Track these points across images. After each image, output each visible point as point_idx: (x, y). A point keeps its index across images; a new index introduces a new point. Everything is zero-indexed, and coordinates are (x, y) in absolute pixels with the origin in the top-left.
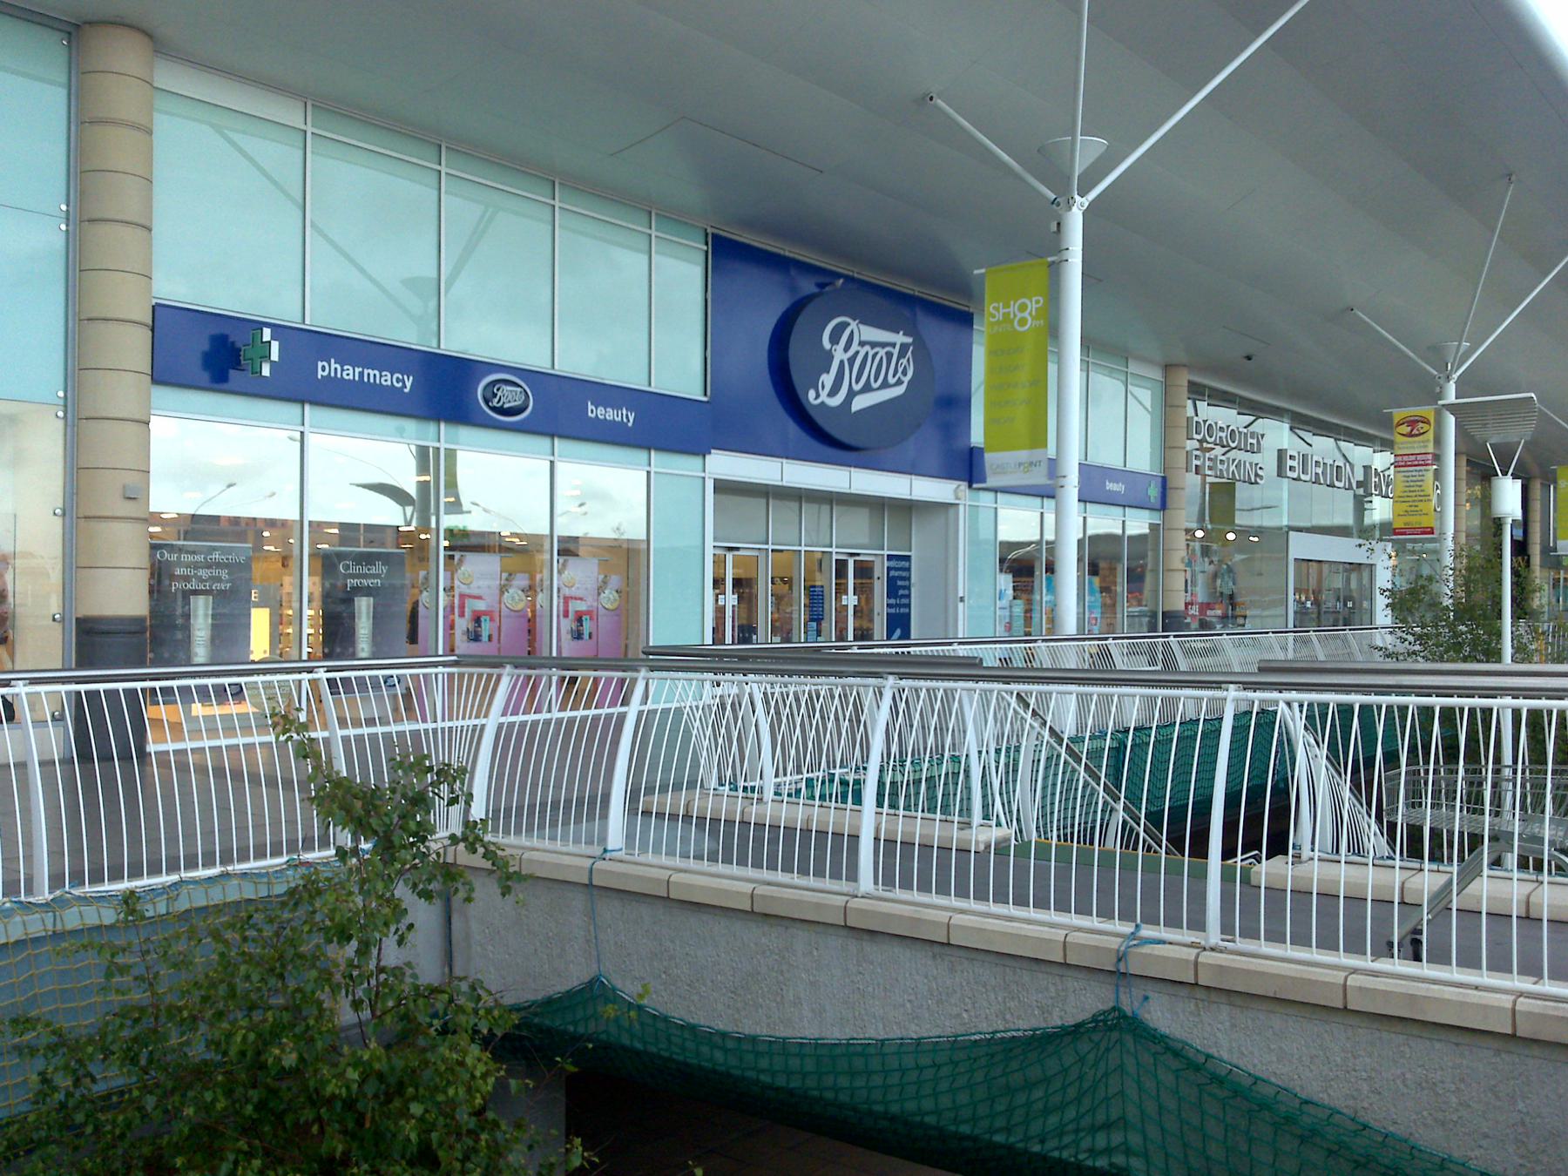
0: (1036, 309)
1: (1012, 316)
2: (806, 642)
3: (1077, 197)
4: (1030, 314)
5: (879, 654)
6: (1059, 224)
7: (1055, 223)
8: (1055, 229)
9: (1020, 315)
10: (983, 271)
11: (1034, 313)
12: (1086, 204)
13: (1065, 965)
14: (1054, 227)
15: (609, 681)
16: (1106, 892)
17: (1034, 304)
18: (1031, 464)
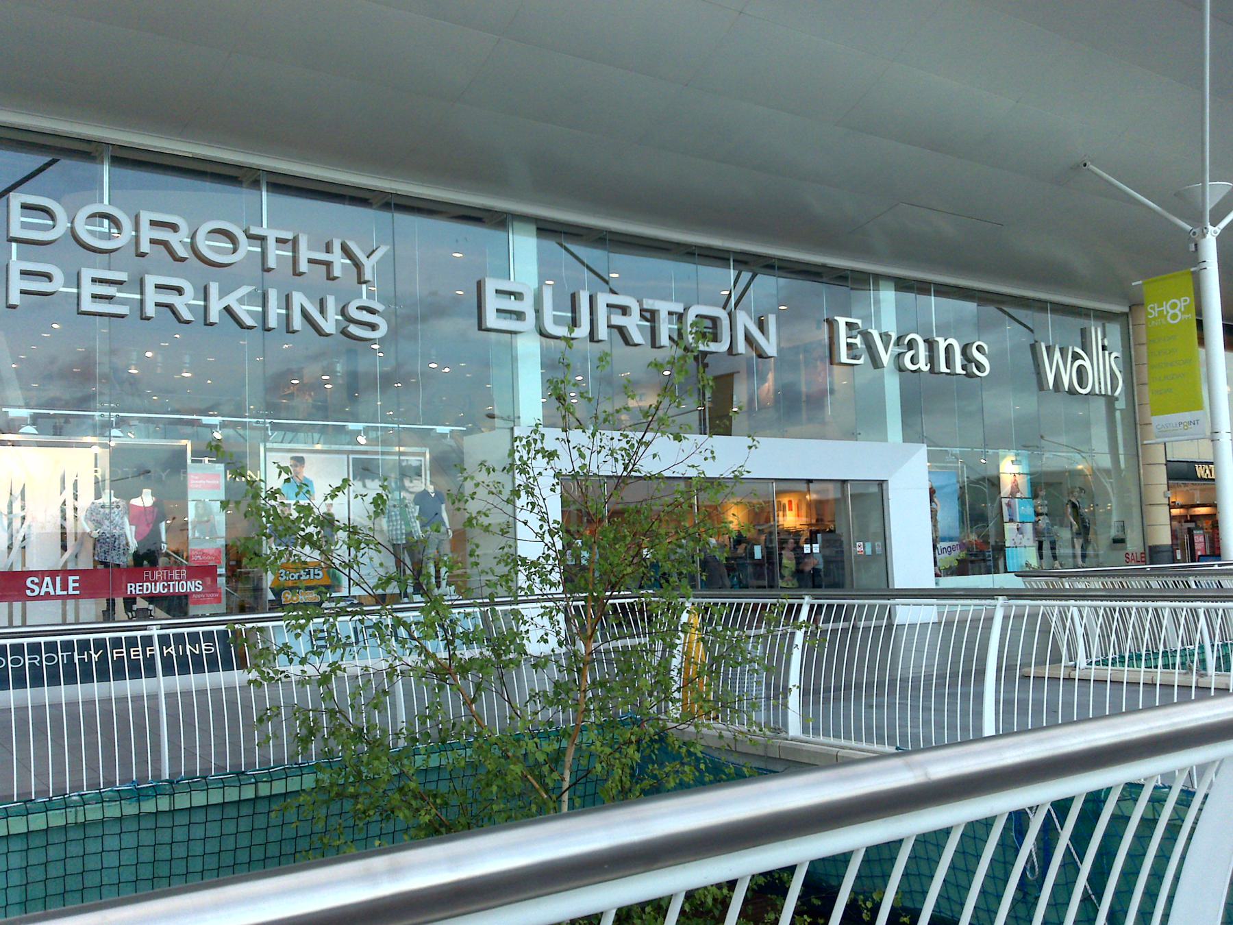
0: (1185, 306)
1: (1165, 313)
2: (24, 625)
3: (1210, 228)
4: (1180, 310)
5: (1227, 569)
6: (1196, 245)
7: (1193, 245)
8: (1194, 249)
9: (1171, 312)
10: (1140, 282)
11: (1183, 309)
12: (1219, 231)
13: (780, 759)
14: (1192, 248)
15: (756, 605)
16: (837, 725)
17: (1186, 301)
18: (1190, 422)
